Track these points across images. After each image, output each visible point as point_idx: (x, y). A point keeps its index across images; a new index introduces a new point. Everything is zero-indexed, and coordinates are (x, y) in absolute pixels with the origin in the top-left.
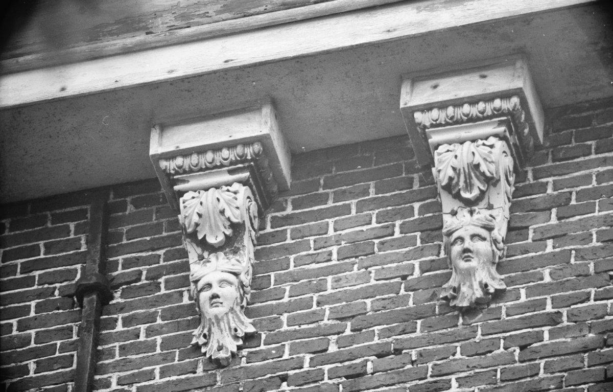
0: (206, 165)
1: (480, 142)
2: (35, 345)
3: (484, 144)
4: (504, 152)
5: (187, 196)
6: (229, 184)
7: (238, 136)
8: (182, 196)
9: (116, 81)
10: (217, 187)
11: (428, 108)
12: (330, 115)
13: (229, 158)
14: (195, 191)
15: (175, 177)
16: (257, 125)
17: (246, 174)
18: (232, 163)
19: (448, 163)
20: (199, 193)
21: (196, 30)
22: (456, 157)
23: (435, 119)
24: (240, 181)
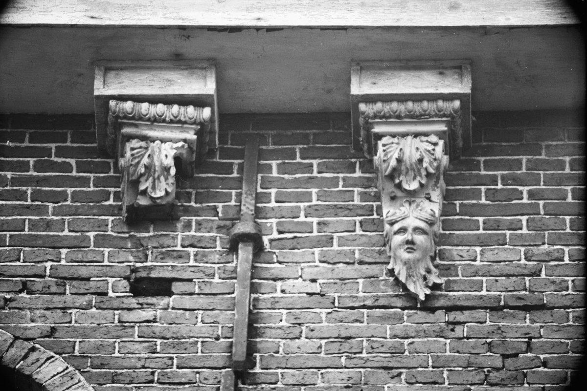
17: (443, 128)
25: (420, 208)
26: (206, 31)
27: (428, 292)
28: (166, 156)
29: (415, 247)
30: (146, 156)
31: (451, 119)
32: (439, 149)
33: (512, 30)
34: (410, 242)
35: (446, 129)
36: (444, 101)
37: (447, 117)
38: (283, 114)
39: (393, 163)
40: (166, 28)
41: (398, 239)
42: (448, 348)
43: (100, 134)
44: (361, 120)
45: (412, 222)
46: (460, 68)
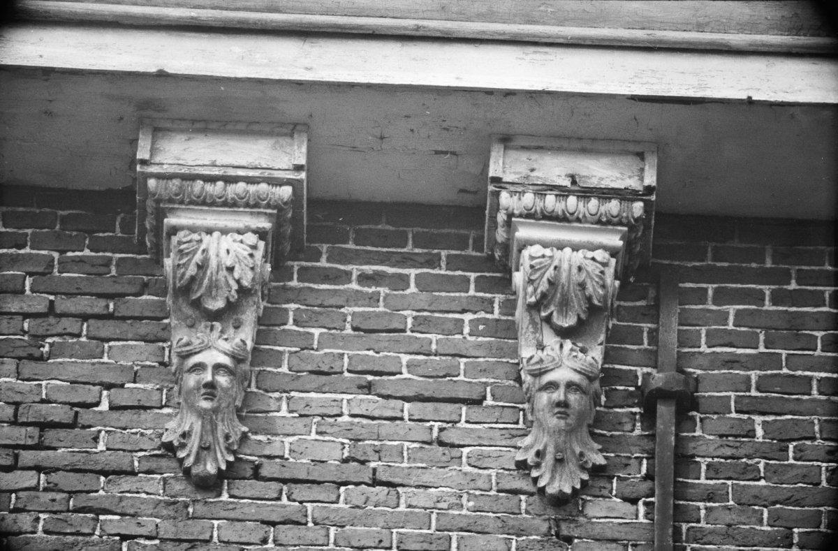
9: (41, 56)
12: (399, 170)
13: (245, 197)
17: (265, 224)
21: (123, 10)
25: (225, 337)
26: (481, 95)
27: (585, 477)
28: (228, 252)
29: (569, 411)
30: (552, 268)
31: (633, 228)
32: (610, 271)
33: (509, 97)
34: (211, 386)
35: (621, 243)
36: (599, 198)
37: (273, 209)
38: (386, 209)
39: (544, 286)
40: (164, 76)
41: (544, 398)
42: (40, 527)
43: (122, 215)
44: (150, 203)
45: (211, 357)
46: (641, 156)
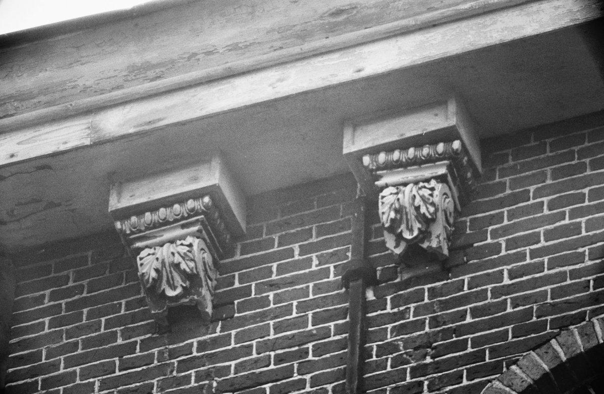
0: (130, 230)
1: (179, 242)
2: (152, 381)
3: (425, 187)
4: (202, 249)
5: (143, 254)
6: (183, 237)
7: (409, 134)
8: (139, 254)
10: (172, 241)
11: (374, 151)
12: (279, 162)
14: (151, 248)
15: (131, 237)
16: (211, 176)
18: (183, 218)
19: (151, 266)
20: (155, 249)
22: (157, 259)
23: (177, 214)
24: (193, 235)
